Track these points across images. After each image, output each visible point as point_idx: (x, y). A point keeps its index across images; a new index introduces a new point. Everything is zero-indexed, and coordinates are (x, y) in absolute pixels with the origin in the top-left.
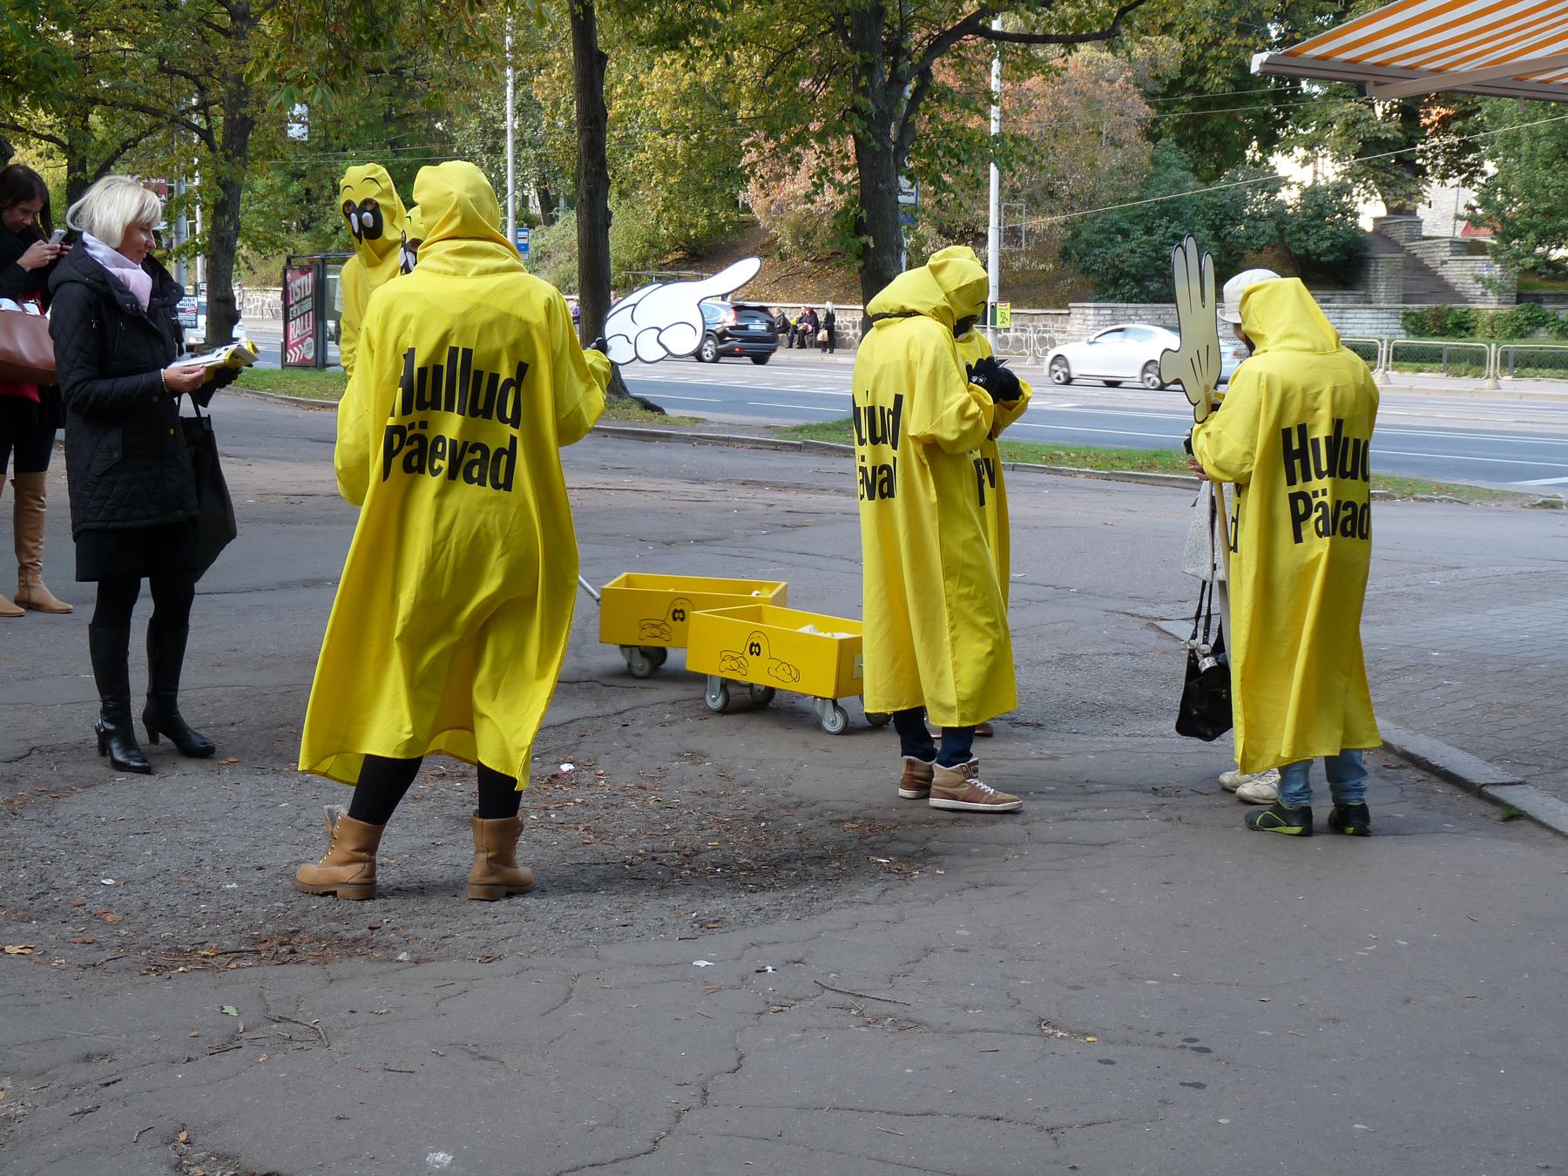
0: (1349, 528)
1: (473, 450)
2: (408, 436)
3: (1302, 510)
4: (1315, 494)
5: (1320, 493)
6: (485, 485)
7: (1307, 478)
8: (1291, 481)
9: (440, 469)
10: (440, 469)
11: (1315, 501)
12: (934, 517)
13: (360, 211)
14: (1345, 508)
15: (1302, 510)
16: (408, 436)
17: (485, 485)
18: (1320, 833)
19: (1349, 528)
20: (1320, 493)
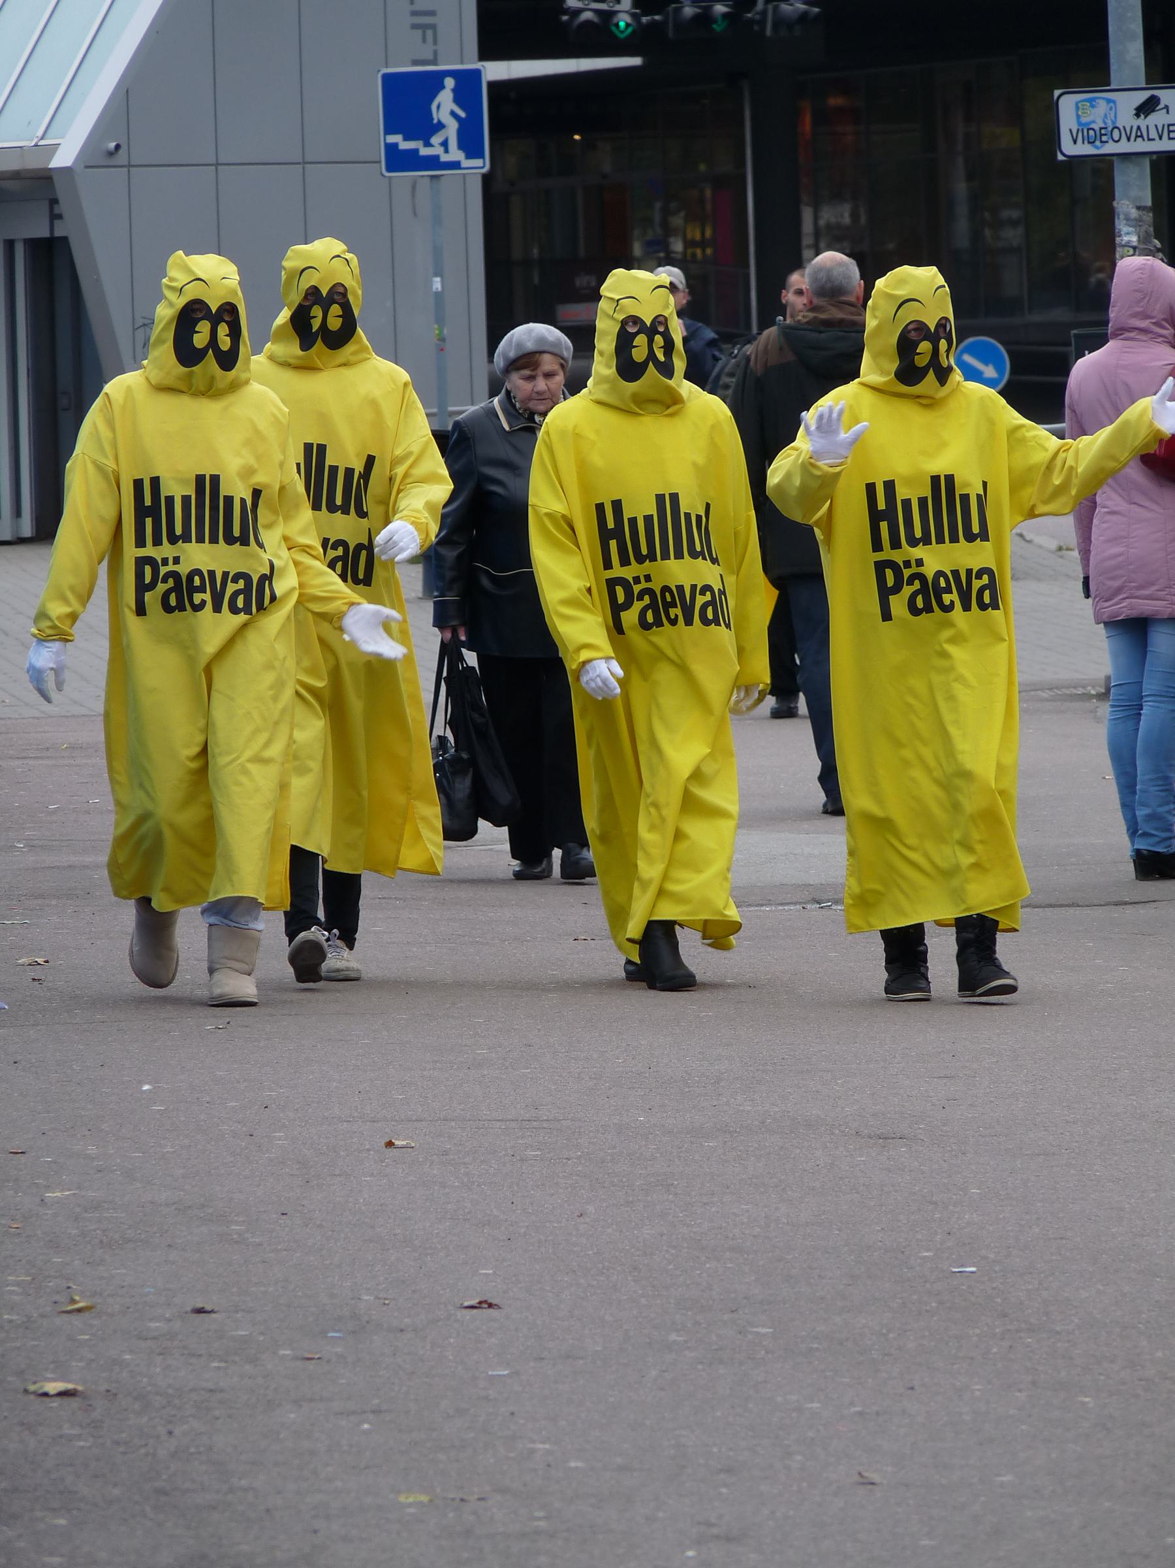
0: (710, 616)
1: (979, 576)
2: (162, 574)
3: (890, 582)
4: (907, 564)
5: (171, 561)
6: (933, 611)
7: (896, 544)
8: (140, 542)
9: (204, 602)
10: (204, 602)
11: (163, 570)
12: (1127, 616)
13: (215, 320)
14: (703, 593)
15: (890, 582)
16: (162, 574)
17: (933, 611)
18: (944, 1002)
19: (710, 616)
20: (171, 561)
